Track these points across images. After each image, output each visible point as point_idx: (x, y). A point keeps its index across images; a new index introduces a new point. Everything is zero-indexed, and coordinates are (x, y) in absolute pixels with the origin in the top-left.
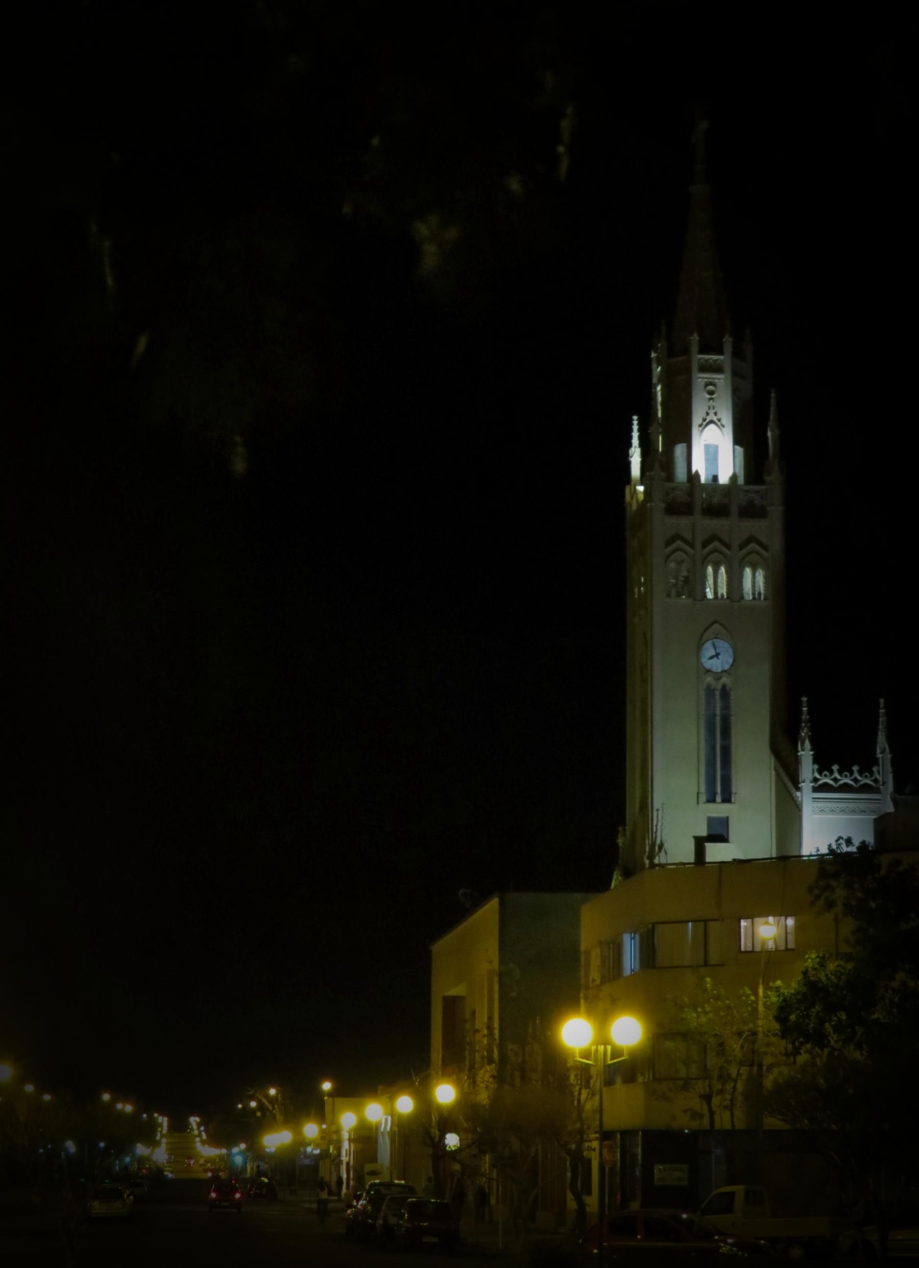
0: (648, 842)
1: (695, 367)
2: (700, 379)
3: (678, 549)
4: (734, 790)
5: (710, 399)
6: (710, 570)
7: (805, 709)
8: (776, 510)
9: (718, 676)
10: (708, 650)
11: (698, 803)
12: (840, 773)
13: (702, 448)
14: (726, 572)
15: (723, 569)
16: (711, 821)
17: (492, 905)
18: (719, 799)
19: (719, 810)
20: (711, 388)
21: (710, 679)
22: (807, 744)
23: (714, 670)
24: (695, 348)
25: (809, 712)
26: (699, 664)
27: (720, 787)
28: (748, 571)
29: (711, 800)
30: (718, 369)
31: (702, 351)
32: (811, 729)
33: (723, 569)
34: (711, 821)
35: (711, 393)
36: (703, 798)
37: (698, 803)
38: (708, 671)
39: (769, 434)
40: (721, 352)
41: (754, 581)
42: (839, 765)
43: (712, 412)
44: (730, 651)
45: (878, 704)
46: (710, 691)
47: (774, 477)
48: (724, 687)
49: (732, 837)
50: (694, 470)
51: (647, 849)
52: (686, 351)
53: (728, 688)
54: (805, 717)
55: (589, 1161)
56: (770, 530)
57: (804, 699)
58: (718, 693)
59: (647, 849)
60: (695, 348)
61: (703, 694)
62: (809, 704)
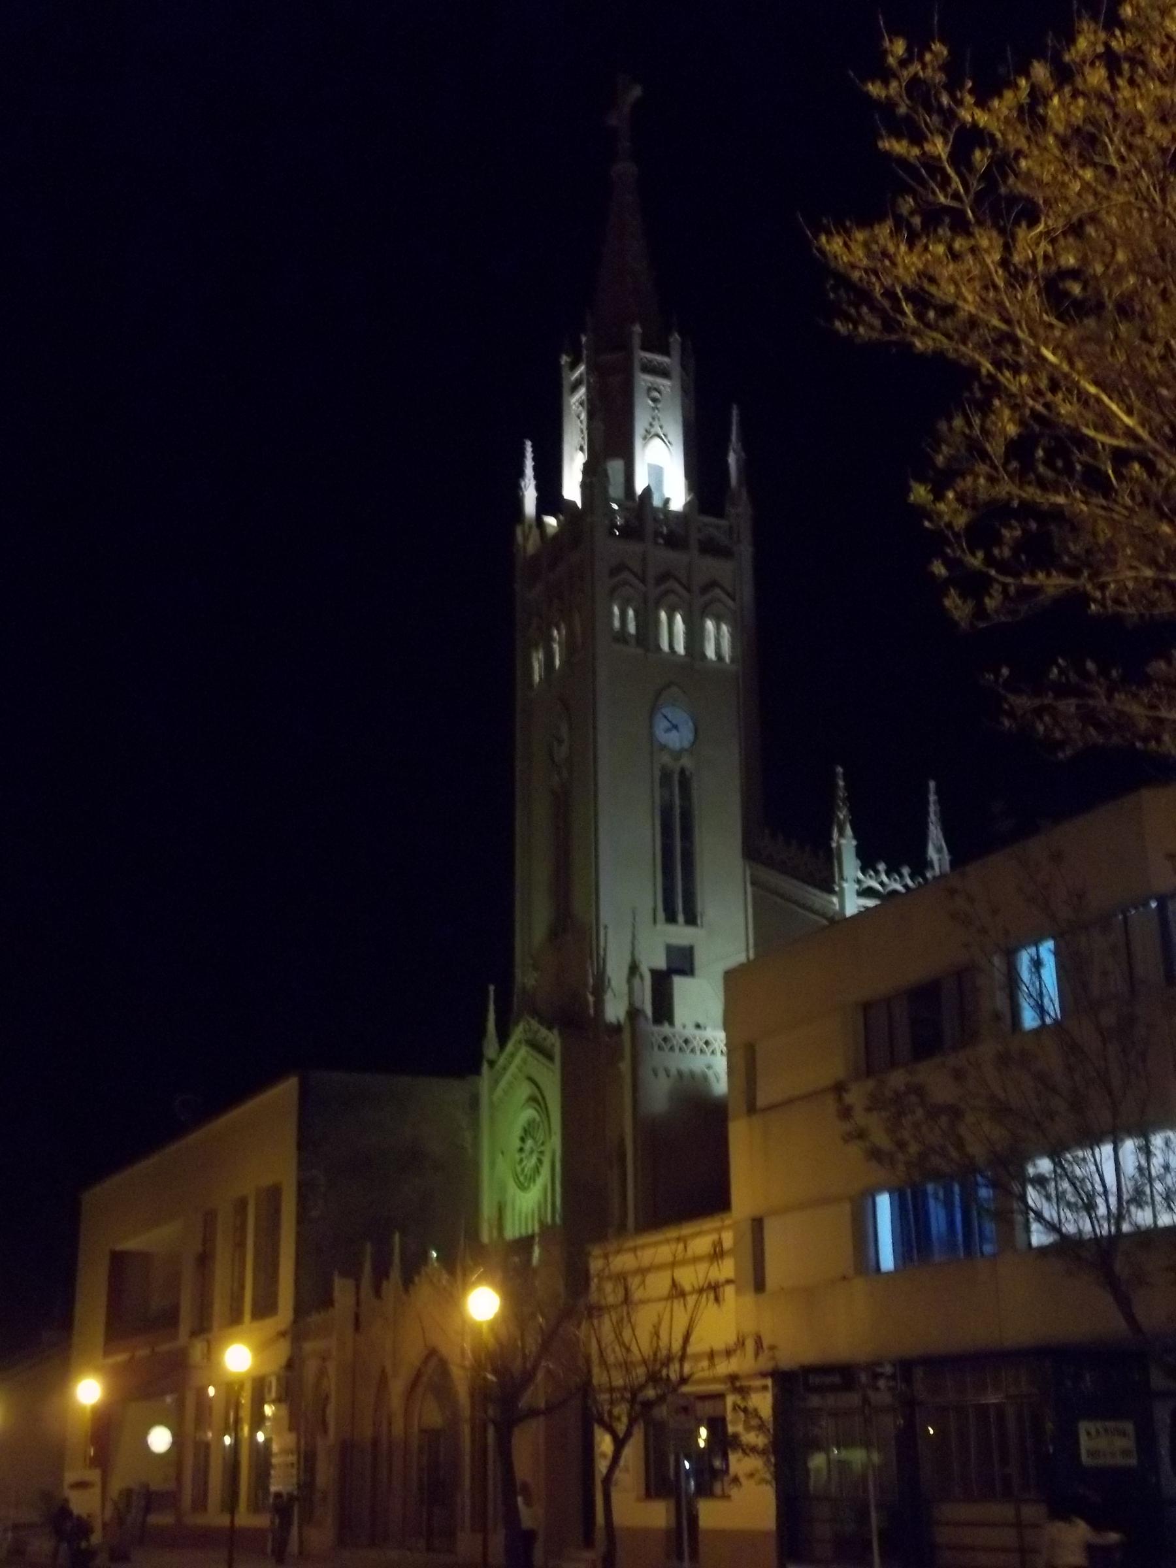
0: (591, 972)
1: (637, 365)
2: (644, 380)
3: (626, 583)
4: (699, 908)
5: (653, 409)
6: (663, 615)
7: (841, 783)
8: (746, 550)
9: (677, 755)
10: (661, 725)
11: (655, 921)
12: (888, 874)
13: (646, 467)
14: (684, 621)
15: (678, 618)
16: (671, 950)
17: (286, 1090)
18: (681, 918)
19: (681, 934)
20: (656, 394)
21: (666, 759)
22: (849, 831)
23: (671, 745)
24: (637, 341)
25: (846, 788)
26: (652, 736)
27: (679, 900)
28: (710, 625)
29: (671, 918)
30: (664, 373)
31: (645, 348)
32: (851, 811)
33: (678, 618)
34: (671, 950)
35: (654, 400)
36: (661, 915)
37: (655, 921)
38: (663, 747)
39: (732, 459)
40: (667, 353)
41: (718, 640)
42: (886, 863)
43: (656, 423)
44: (691, 724)
45: (927, 786)
46: (666, 777)
47: (741, 511)
48: (682, 771)
49: (697, 972)
50: (639, 488)
51: (591, 981)
52: (624, 347)
53: (687, 773)
54: (841, 793)
55: (270, 1383)
56: (736, 573)
57: (840, 770)
58: (676, 777)
59: (591, 981)
60: (637, 341)
61: (657, 774)
62: (846, 777)
